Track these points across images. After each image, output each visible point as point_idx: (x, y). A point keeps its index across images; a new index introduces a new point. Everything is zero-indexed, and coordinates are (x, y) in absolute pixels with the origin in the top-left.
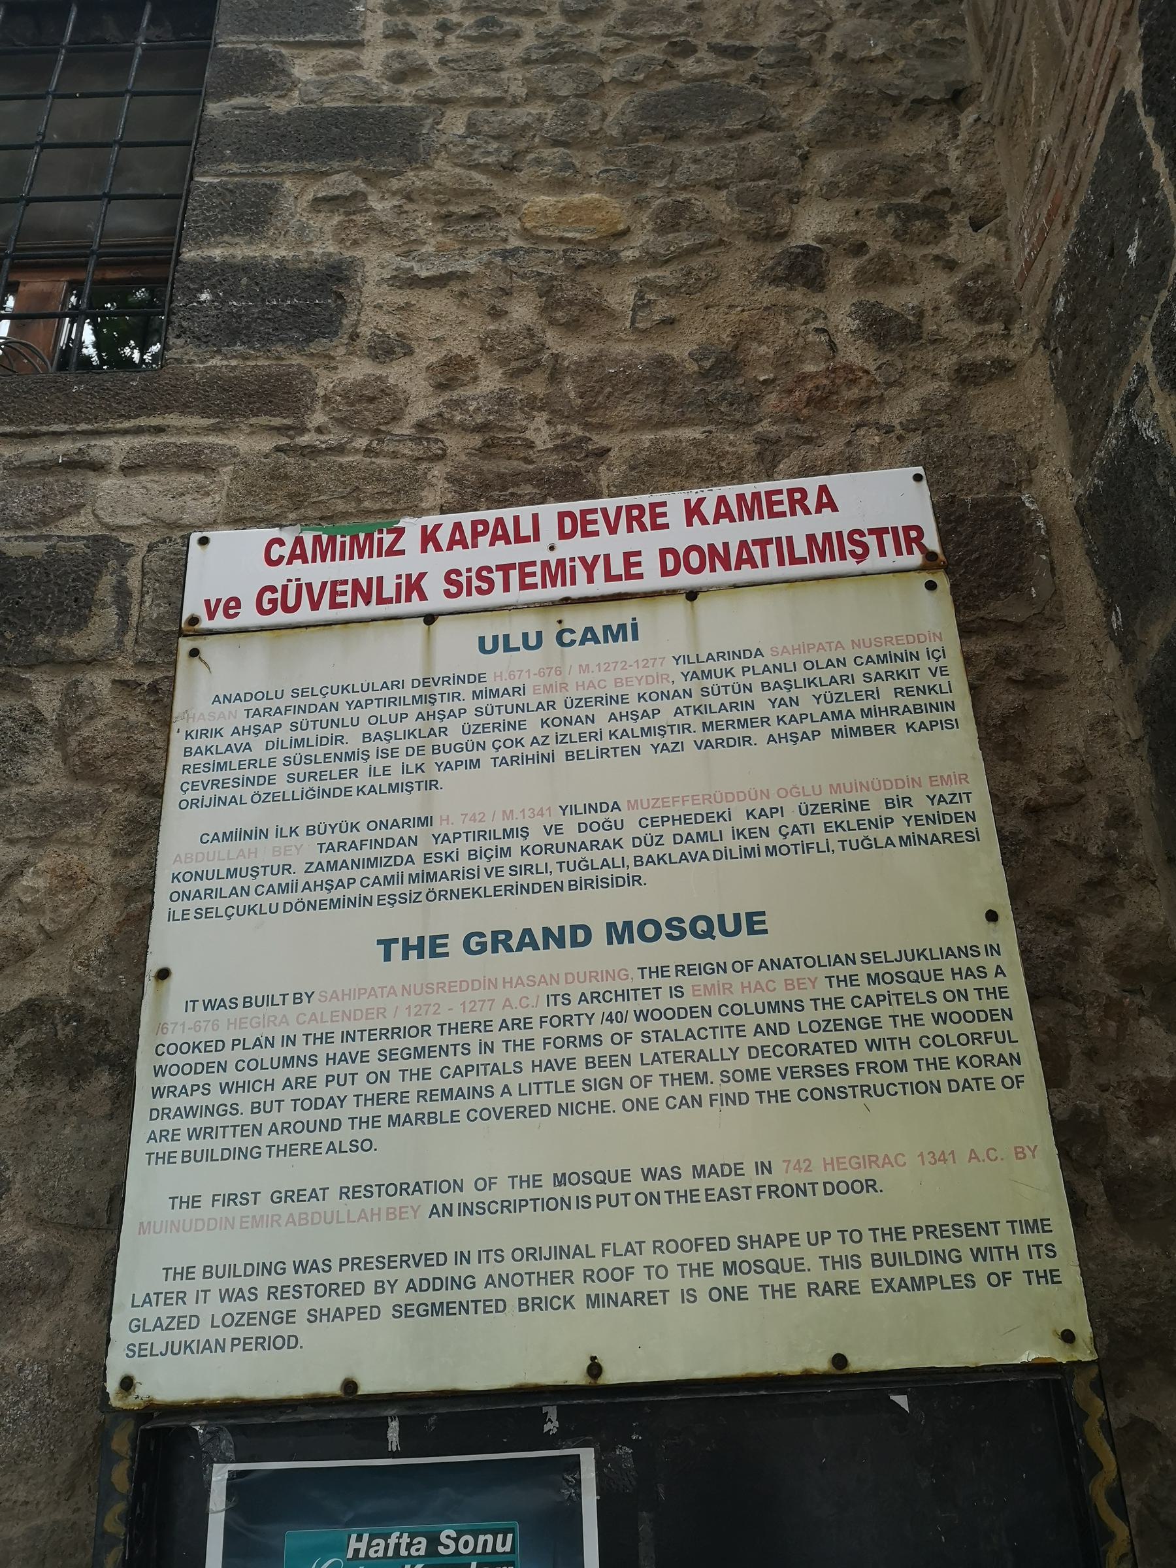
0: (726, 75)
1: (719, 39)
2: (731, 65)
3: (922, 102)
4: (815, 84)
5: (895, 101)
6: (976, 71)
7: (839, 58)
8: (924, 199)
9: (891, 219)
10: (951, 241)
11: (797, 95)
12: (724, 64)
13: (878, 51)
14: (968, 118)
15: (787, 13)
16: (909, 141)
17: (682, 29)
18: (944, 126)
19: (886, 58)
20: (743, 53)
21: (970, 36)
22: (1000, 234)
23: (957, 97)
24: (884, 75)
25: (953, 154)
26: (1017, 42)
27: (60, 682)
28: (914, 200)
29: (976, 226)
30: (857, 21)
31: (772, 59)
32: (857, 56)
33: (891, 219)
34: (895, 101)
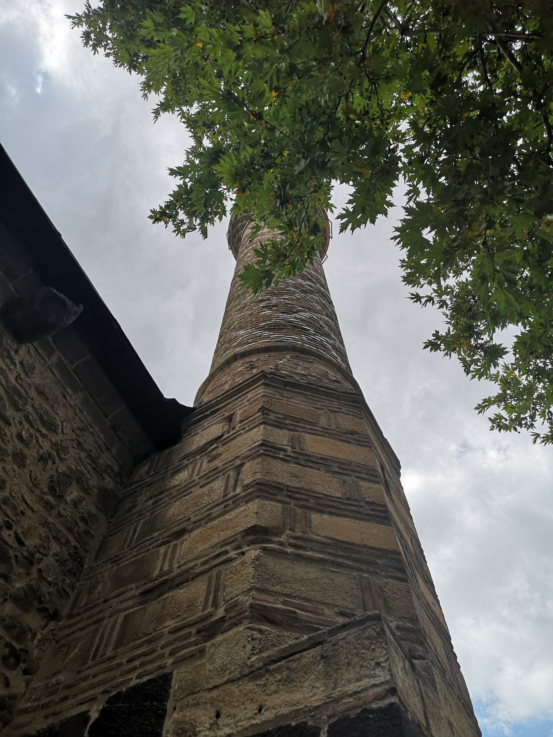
0: (11, 547)
1: (19, 532)
2: (16, 545)
3: (46, 610)
4: (28, 574)
5: (41, 602)
6: (65, 612)
7: (40, 571)
8: (20, 649)
9: (7, 650)
10: (15, 673)
11: (21, 574)
12: (14, 543)
13: (50, 579)
14: (52, 625)
15: (41, 539)
16: (33, 620)
17: (14, 519)
18: (43, 623)
19: (50, 583)
20: (21, 543)
21: (72, 596)
22: (28, 683)
23: (55, 616)
24: (45, 589)
25: (39, 636)
26: (80, 630)
27: (246, 35)
28: (17, 646)
29: (25, 672)
30: (53, 560)
31: (26, 554)
32: (44, 576)
33: (7, 650)
34: (41, 602)
